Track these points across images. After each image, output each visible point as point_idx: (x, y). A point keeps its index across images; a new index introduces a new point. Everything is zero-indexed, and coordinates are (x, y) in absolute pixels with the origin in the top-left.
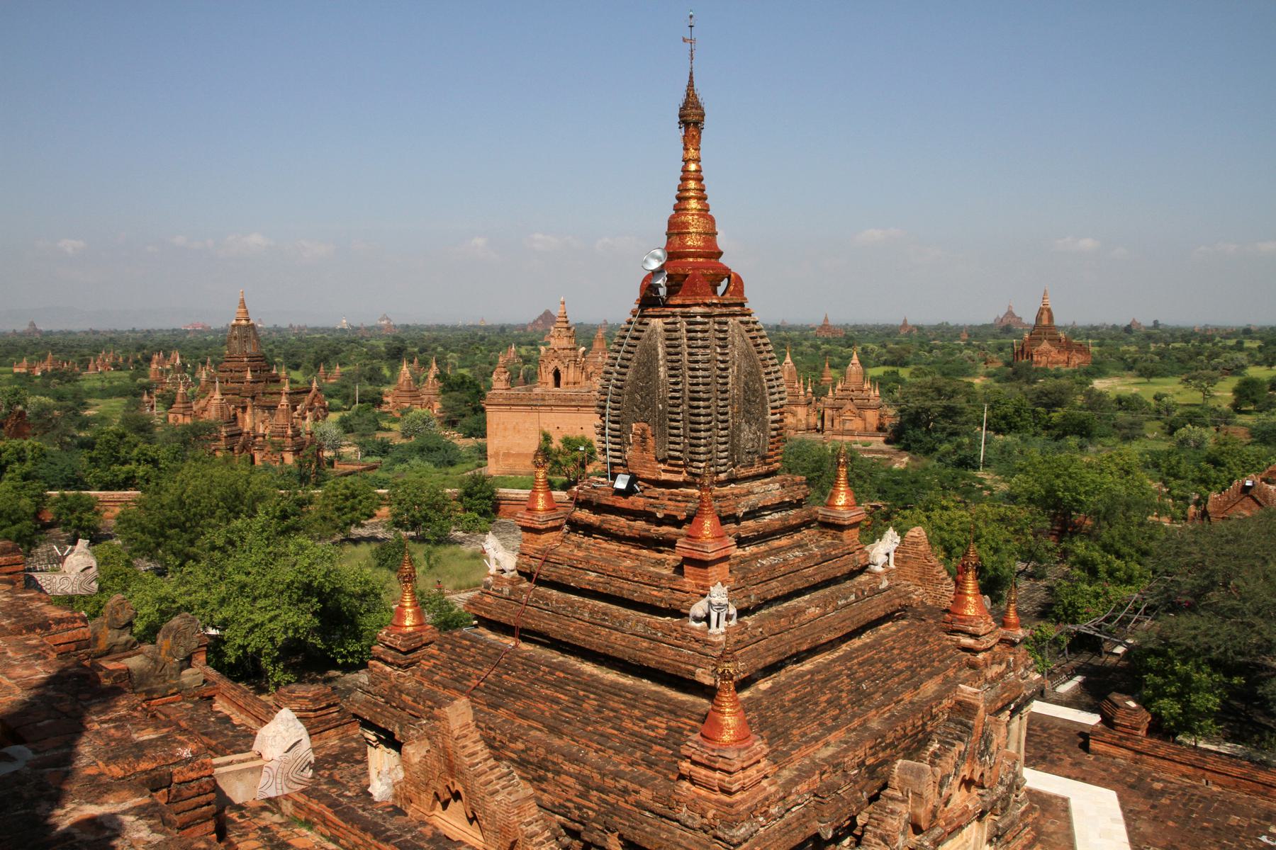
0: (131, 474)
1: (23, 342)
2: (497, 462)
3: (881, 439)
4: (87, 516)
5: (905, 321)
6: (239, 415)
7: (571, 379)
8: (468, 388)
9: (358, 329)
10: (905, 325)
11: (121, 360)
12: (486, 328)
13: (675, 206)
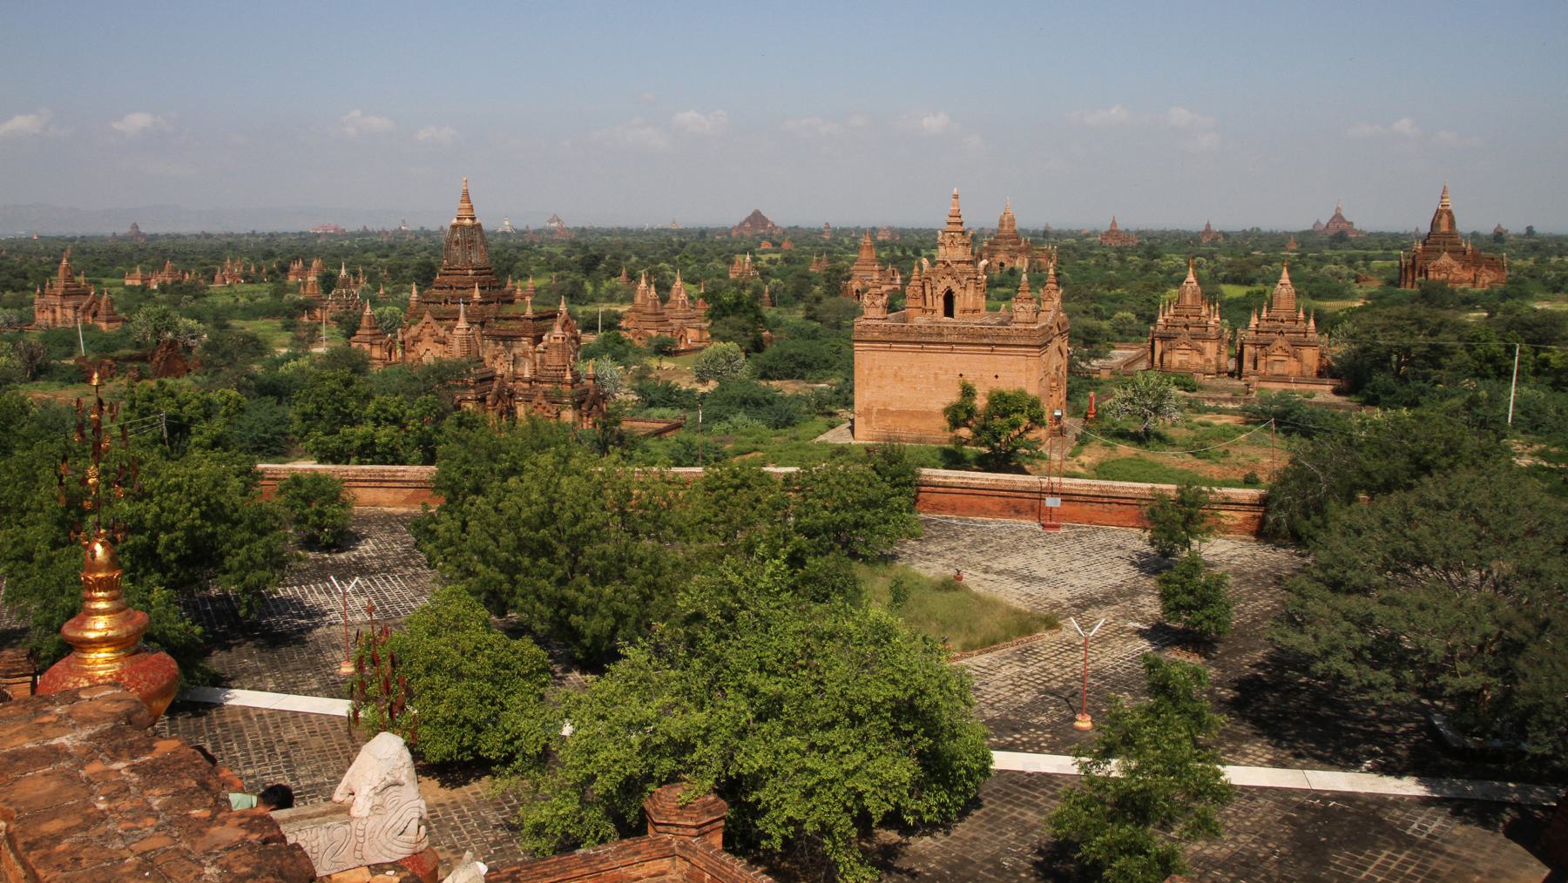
0: (368, 440)
1: (127, 247)
2: (868, 422)
3: (1328, 388)
4: (328, 509)
5: (1208, 225)
7: (970, 305)
8: (745, 312)
9: (523, 232)
10: (1208, 231)
11: (253, 269)
12: (680, 233)
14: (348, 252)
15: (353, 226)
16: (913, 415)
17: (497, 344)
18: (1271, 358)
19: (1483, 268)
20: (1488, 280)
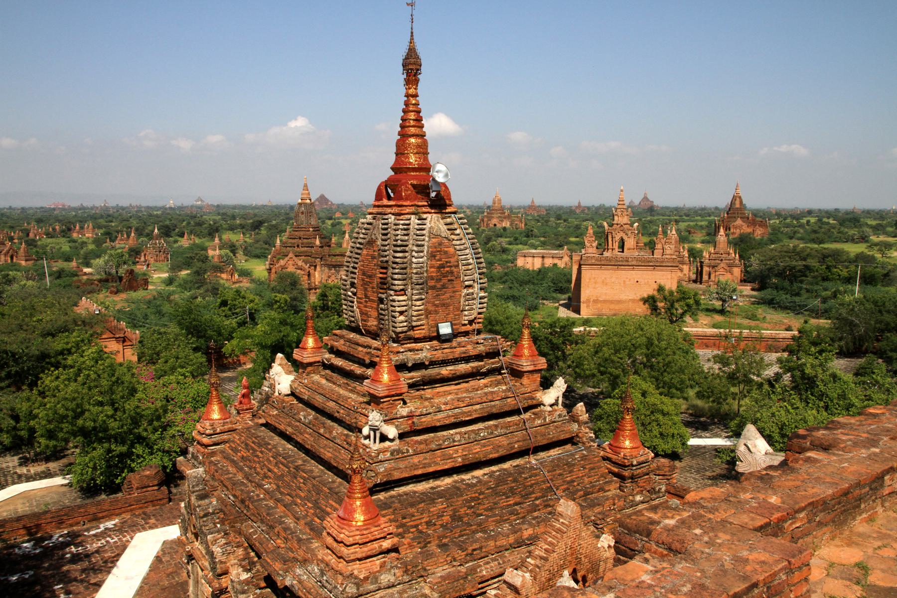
2: (588, 306)
3: (749, 288)
5: (579, 203)
6: (312, 272)
10: (579, 206)
13: (402, 117)
14: (94, 218)
15: (75, 204)
16: (612, 302)
17: (330, 270)
18: (717, 273)
19: (757, 226)
20: (759, 233)
